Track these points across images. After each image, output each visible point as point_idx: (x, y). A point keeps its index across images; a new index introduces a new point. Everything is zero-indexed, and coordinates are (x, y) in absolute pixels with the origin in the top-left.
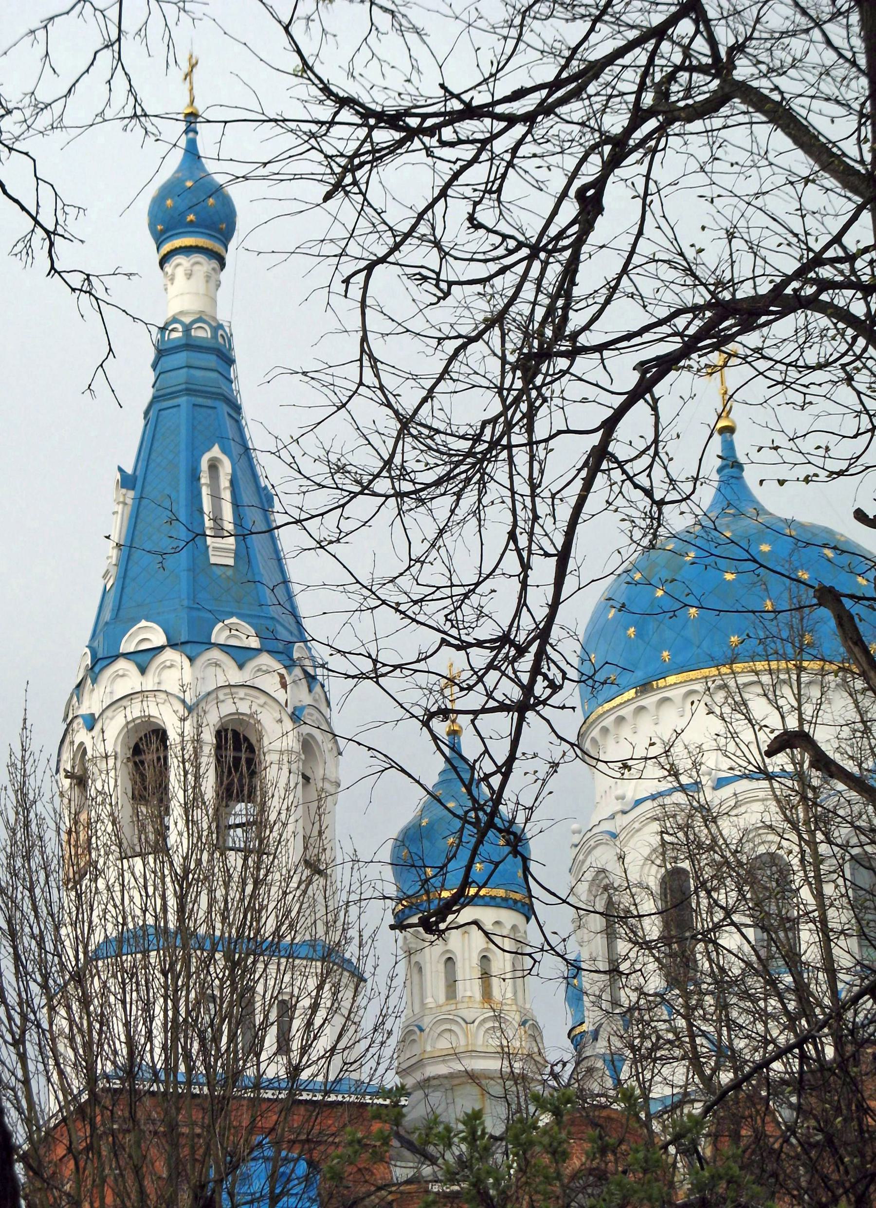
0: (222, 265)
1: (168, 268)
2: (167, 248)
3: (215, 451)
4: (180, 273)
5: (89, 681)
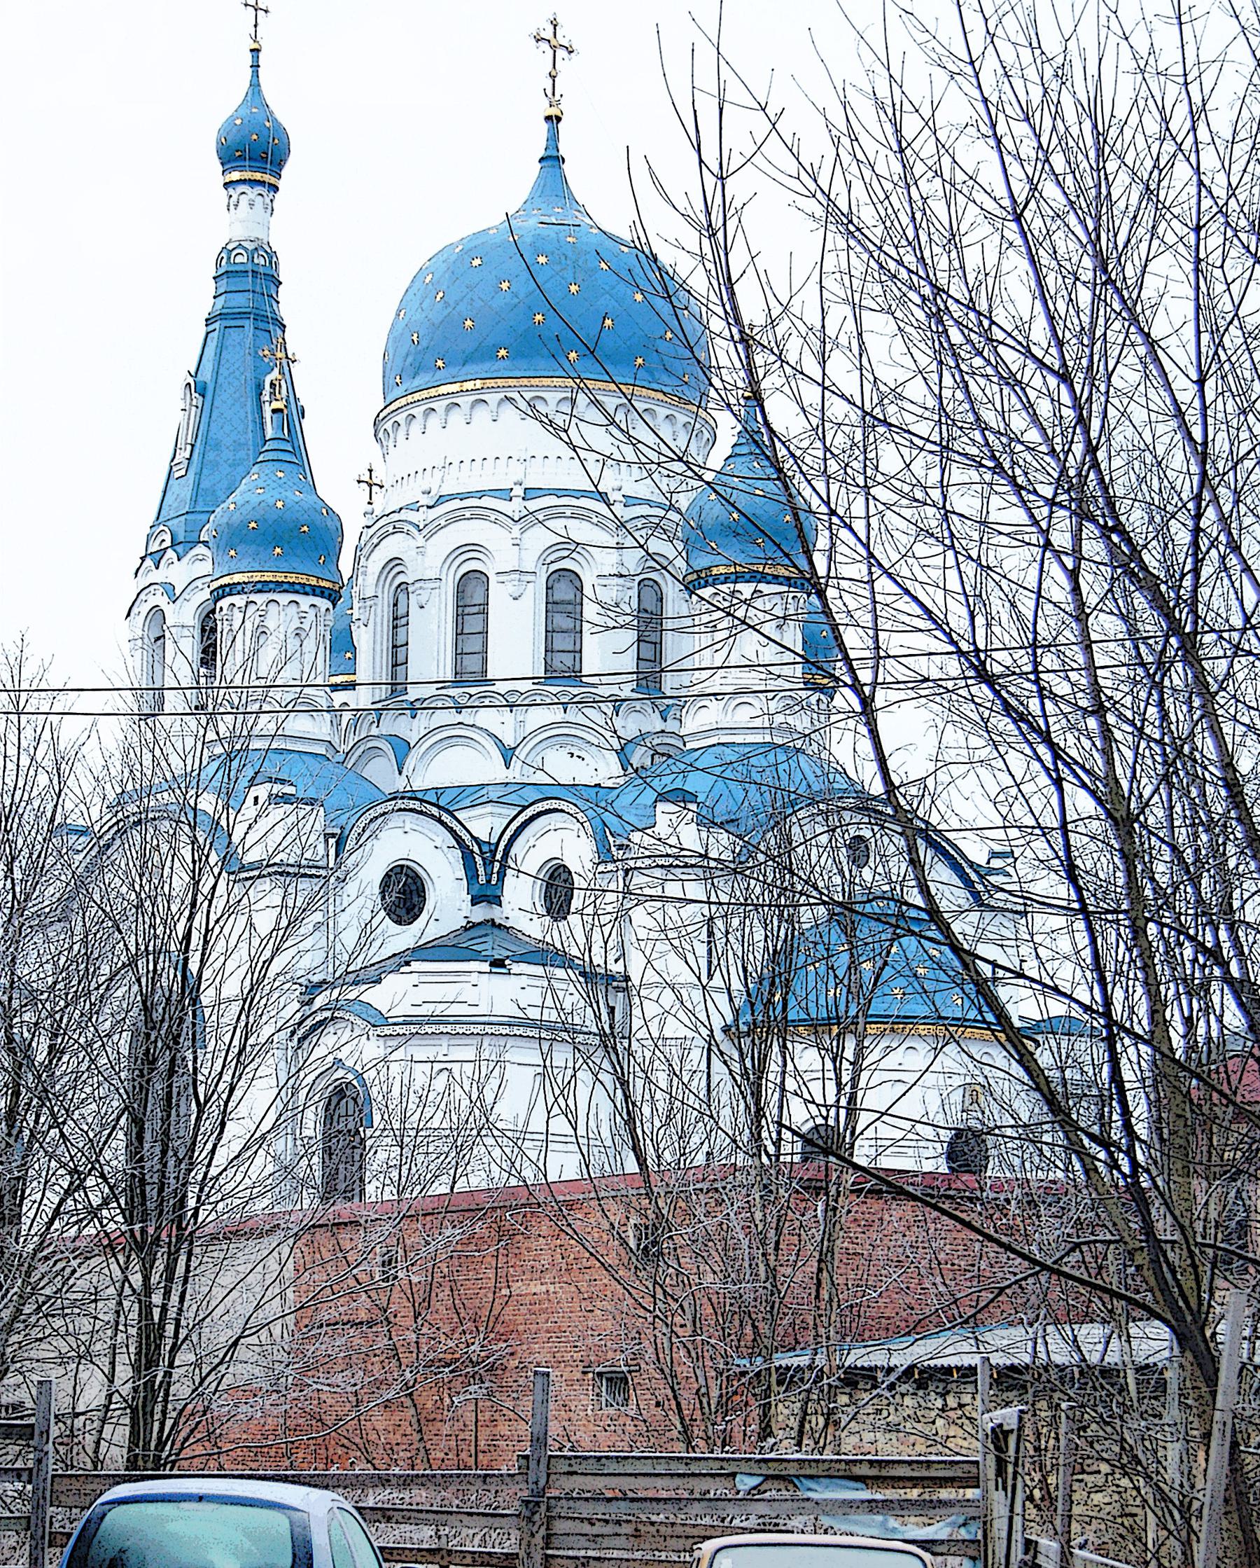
0: (275, 188)
1: (230, 190)
2: (236, 176)
3: (275, 374)
4: (244, 200)
5: (170, 554)
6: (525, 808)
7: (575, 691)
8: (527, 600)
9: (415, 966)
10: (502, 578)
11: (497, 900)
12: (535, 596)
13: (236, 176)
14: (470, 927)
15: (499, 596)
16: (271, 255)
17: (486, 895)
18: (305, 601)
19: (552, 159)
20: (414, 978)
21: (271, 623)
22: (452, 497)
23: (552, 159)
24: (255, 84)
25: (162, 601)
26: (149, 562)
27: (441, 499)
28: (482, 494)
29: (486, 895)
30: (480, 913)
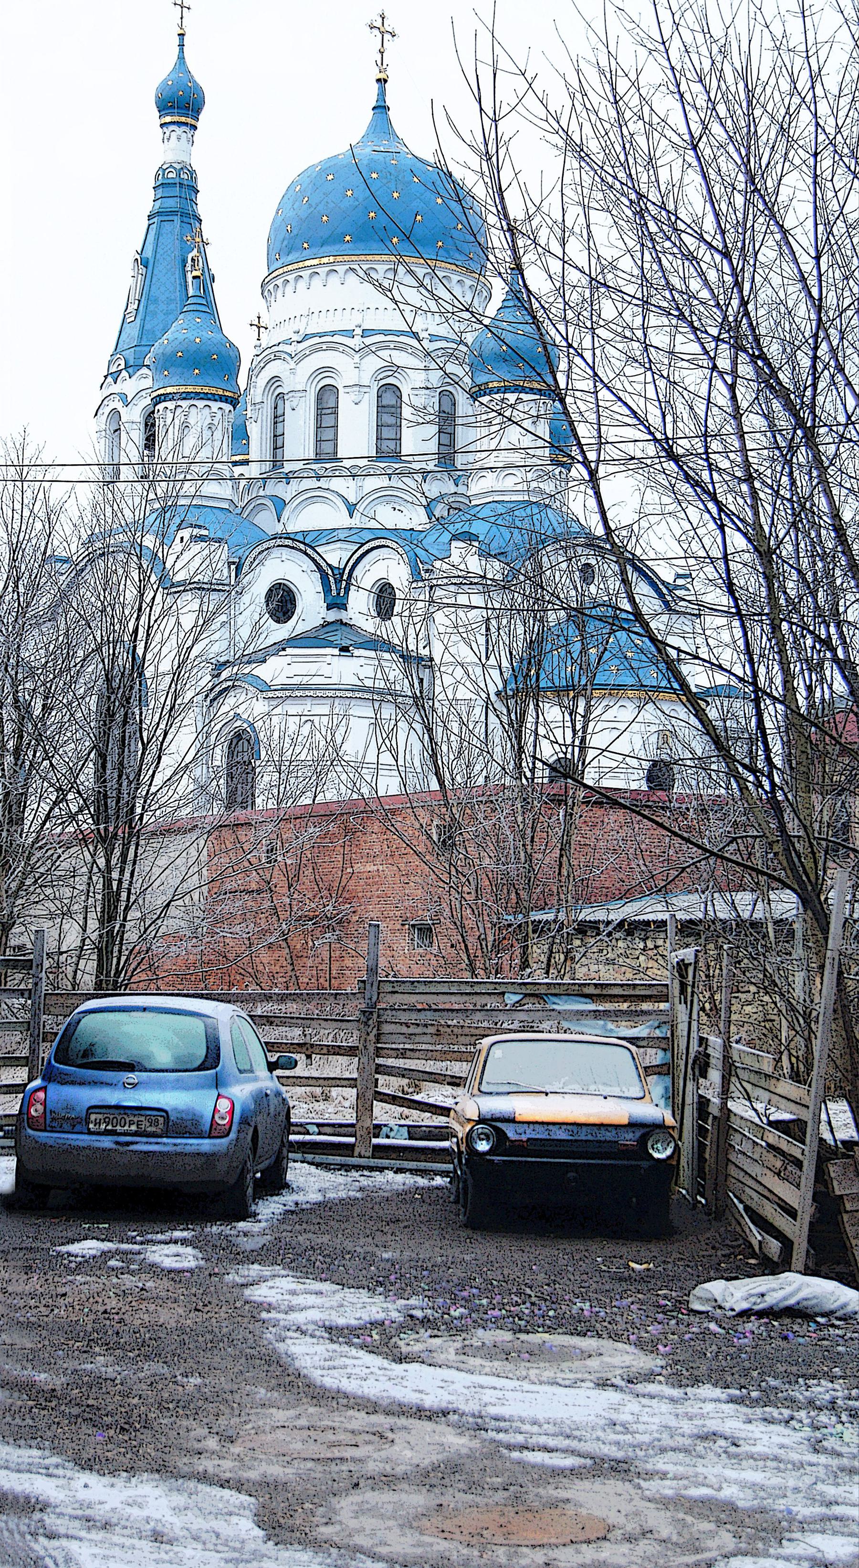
2: (168, 119)
3: (195, 253)
5: (124, 374)
6: (363, 545)
7: (397, 466)
8: (364, 404)
9: (289, 651)
10: (347, 390)
11: (344, 607)
12: (370, 401)
13: (168, 119)
14: (326, 625)
15: (345, 402)
16: (192, 173)
17: (337, 603)
18: (215, 405)
19: (381, 108)
20: (288, 659)
21: (192, 420)
22: (314, 335)
23: (381, 108)
24: (181, 58)
25: (119, 405)
26: (110, 379)
27: (306, 337)
28: (334, 333)
29: (337, 603)
30: (332, 616)
